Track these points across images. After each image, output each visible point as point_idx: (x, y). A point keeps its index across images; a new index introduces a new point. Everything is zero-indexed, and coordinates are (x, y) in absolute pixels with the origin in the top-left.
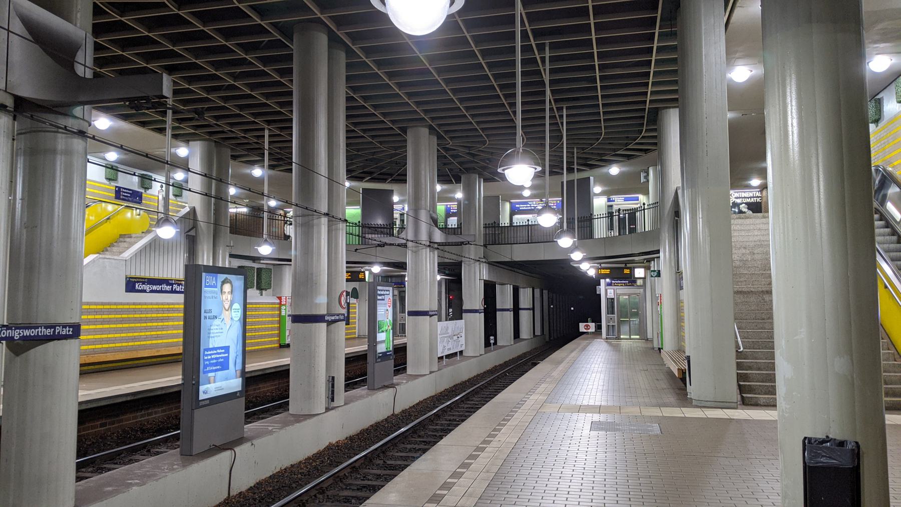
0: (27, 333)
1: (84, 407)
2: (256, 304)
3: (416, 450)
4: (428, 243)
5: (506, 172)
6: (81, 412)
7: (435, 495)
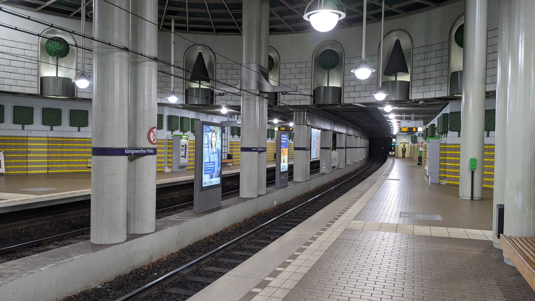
0: (136, 152)
1: (160, 187)
3: (295, 222)
6: (267, 171)
7: (285, 262)
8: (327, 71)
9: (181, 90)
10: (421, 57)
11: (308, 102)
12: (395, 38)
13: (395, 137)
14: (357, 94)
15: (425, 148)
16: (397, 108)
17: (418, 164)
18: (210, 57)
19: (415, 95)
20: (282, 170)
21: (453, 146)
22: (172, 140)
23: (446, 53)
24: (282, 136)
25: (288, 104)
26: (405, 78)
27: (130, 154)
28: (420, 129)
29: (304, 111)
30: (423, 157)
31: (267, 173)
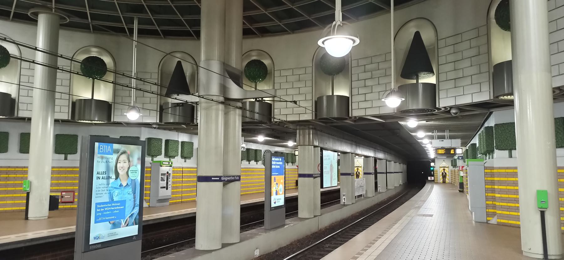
0: (228, 178)
8: (331, 77)
11: (308, 116)
12: (413, 31)
13: (433, 161)
14: (368, 105)
15: (467, 173)
17: (460, 191)
20: (273, 205)
21: (504, 171)
23: (484, 40)
24: (273, 159)
26: (432, 80)
27: (224, 180)
28: (459, 151)
30: (465, 183)
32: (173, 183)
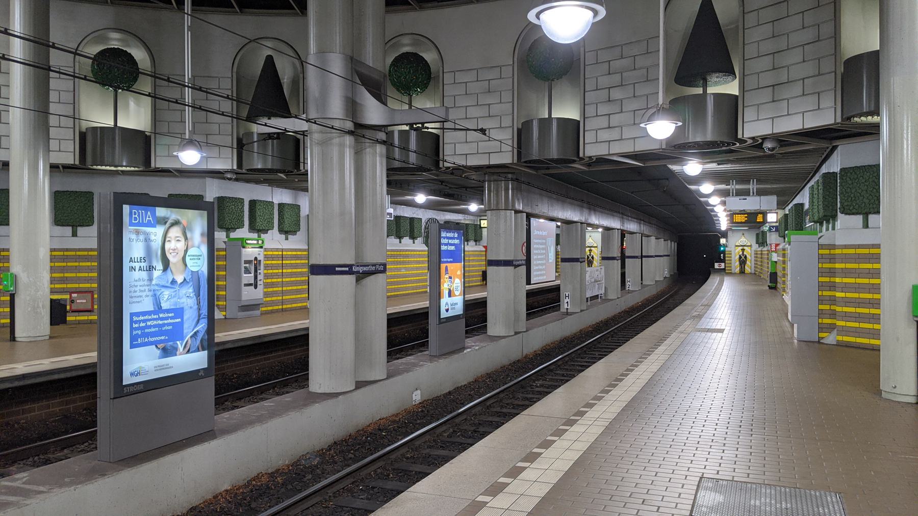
0: (365, 269)
2: (407, 250)
4: (349, 125)
5: (648, 127)
6: (389, 320)
9: (228, 140)
10: (767, 30)
11: (506, 157)
13: (725, 235)
14: (615, 134)
15: (784, 256)
16: (713, 166)
17: (770, 288)
18: (294, 64)
19: (753, 127)
20: (444, 315)
22: (225, 250)
24: (443, 234)
25: (463, 163)
27: (358, 272)
28: (772, 218)
29: (507, 180)
30: (779, 274)
31: (388, 327)
32: (267, 276)
